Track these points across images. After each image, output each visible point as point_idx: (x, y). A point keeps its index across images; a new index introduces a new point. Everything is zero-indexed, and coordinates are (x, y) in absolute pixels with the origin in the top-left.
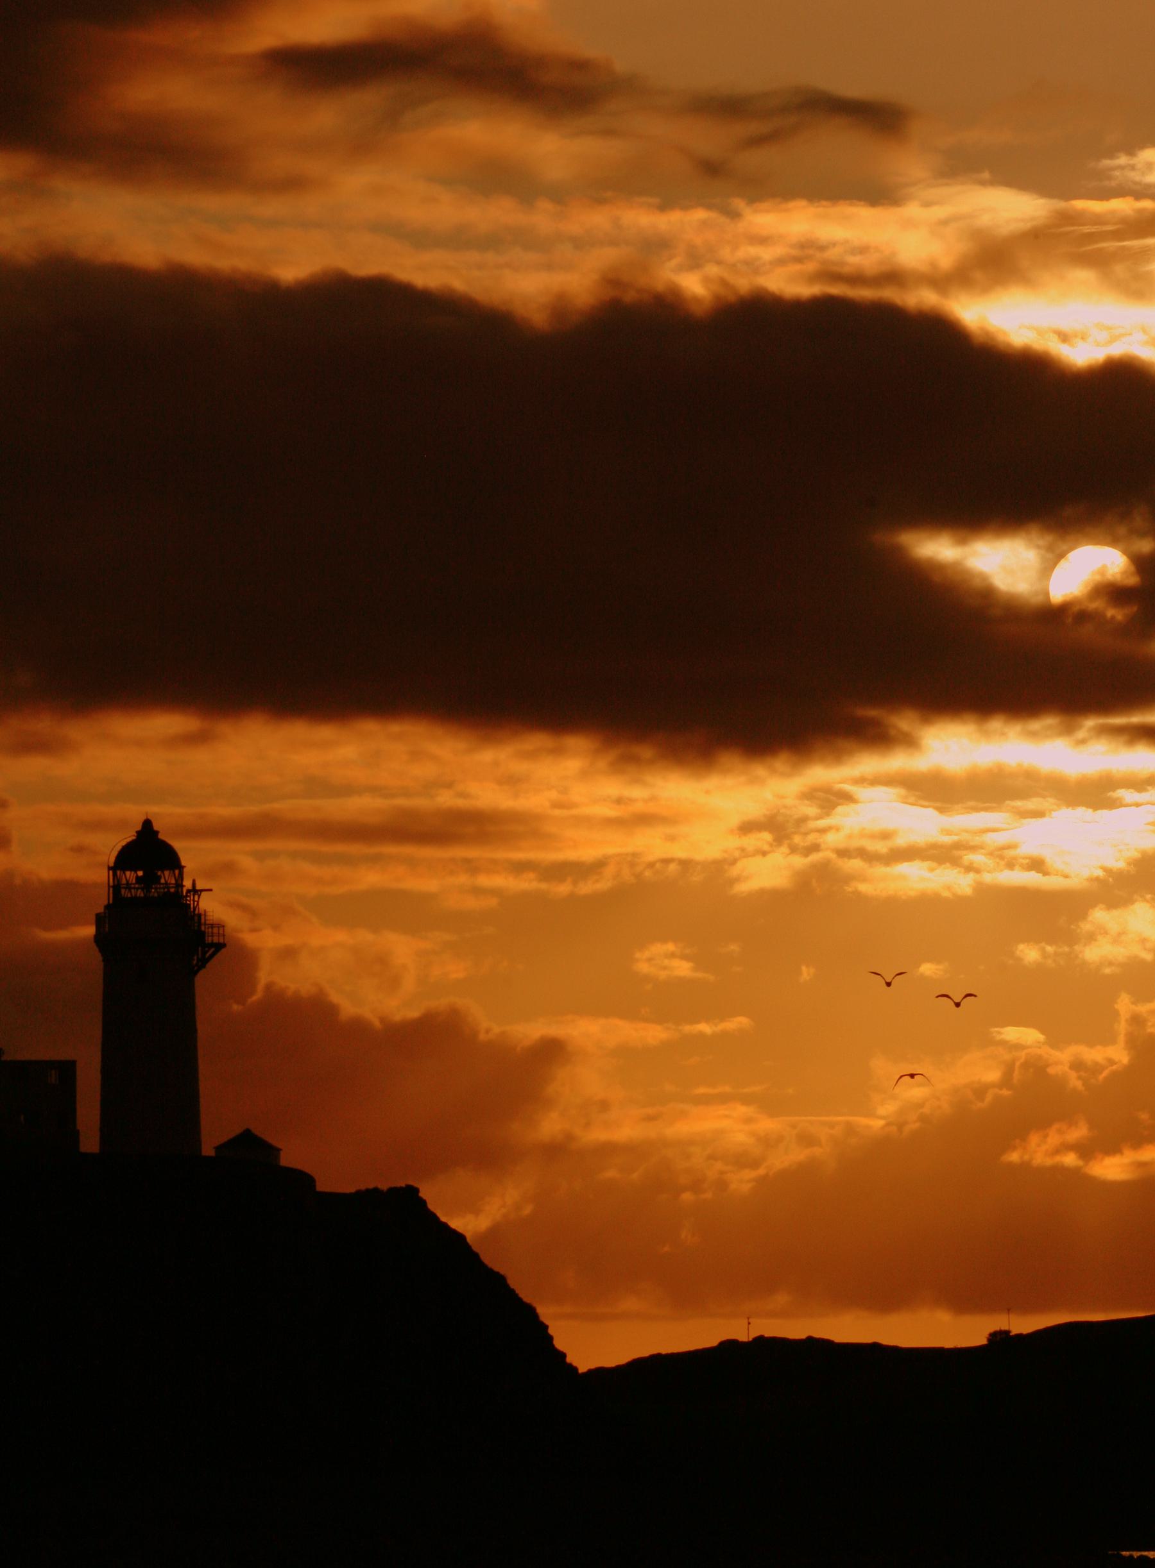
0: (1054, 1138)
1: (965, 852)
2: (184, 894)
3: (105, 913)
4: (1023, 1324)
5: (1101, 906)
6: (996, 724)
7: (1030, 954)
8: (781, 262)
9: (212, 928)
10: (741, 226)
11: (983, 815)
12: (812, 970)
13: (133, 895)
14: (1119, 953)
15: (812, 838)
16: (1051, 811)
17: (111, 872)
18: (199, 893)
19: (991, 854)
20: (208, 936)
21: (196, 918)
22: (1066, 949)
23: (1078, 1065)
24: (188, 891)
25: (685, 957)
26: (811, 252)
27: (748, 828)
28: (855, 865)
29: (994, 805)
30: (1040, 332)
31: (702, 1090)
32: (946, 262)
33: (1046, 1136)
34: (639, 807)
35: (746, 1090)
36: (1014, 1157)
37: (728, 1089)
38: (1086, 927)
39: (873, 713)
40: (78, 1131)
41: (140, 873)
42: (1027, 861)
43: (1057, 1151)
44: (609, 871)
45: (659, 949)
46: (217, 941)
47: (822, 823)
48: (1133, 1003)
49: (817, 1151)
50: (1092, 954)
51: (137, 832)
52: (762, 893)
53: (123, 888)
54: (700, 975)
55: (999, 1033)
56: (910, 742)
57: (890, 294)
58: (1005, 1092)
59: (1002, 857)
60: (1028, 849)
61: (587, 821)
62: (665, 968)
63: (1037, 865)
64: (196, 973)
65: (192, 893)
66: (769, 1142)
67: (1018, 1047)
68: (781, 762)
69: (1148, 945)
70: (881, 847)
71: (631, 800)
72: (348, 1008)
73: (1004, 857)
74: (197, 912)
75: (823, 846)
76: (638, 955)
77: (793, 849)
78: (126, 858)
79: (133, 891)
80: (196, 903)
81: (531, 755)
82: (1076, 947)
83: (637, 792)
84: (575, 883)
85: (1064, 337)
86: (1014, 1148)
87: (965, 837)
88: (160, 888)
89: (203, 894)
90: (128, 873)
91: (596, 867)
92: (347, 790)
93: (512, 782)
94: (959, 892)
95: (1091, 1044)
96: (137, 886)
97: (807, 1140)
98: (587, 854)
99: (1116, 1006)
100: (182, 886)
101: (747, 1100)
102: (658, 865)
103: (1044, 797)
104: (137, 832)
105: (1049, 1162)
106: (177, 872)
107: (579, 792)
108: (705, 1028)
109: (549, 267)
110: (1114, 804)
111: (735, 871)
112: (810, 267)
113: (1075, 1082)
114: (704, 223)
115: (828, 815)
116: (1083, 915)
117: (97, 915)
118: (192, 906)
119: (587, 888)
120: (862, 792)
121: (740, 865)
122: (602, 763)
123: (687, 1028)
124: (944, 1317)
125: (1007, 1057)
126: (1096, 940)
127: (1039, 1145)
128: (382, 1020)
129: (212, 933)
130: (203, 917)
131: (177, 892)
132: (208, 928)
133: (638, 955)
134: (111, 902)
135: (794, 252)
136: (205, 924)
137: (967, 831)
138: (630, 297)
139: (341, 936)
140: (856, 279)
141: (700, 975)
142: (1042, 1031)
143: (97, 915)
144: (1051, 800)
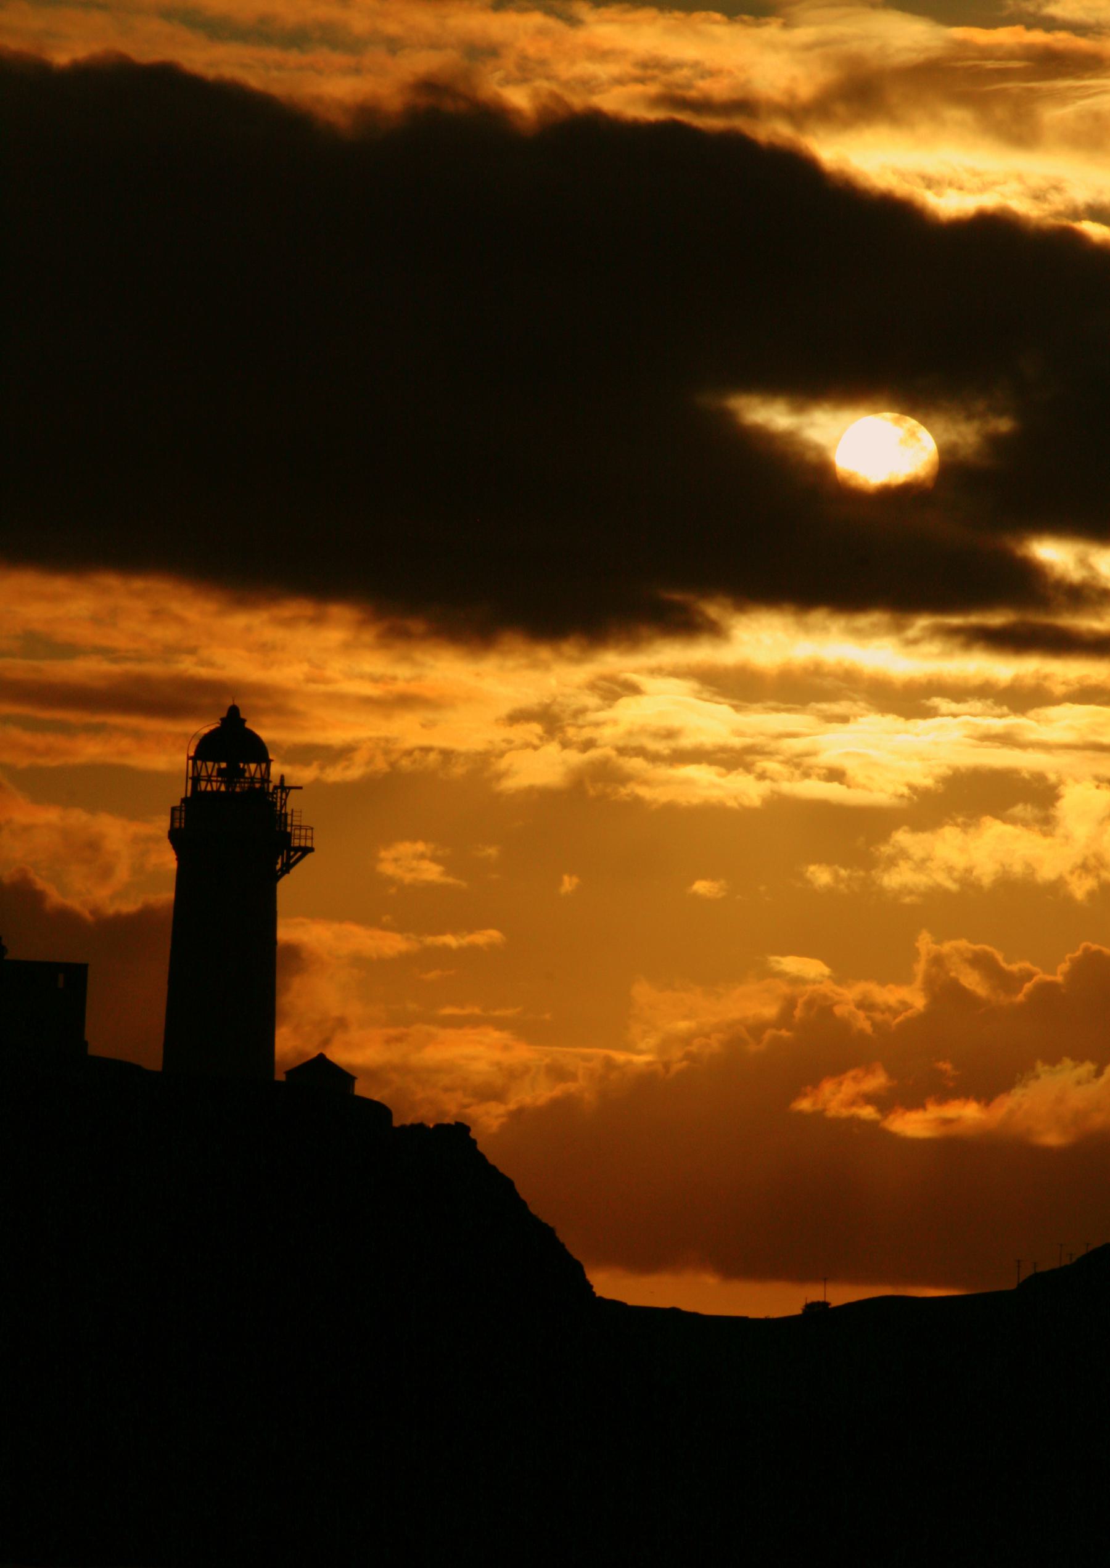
0: (848, 1088)
1: (758, 758)
2: (271, 790)
3: (181, 806)
4: (840, 1295)
5: (906, 828)
6: (818, 617)
7: (821, 876)
8: (619, 81)
9: (300, 829)
10: (580, 36)
11: (784, 716)
12: (575, 880)
13: (215, 789)
14: (920, 880)
15: (587, 733)
16: (855, 716)
17: (190, 762)
18: (288, 791)
19: (786, 762)
20: (294, 839)
21: (283, 817)
22: (862, 873)
23: (865, 1005)
24: (275, 788)
25: (435, 859)
26: (656, 72)
27: (517, 717)
28: (636, 764)
29: (798, 706)
30: (902, 175)
31: (449, 1011)
32: (806, 91)
33: (840, 1084)
34: (400, 687)
35: (497, 1013)
36: (805, 1105)
37: (477, 1011)
38: (886, 850)
39: (677, 597)
40: (86, 1043)
41: (223, 765)
42: (824, 771)
43: (852, 1103)
44: (360, 757)
45: (406, 848)
46: (298, 845)
47: (602, 715)
48: (933, 942)
49: (572, 1087)
50: (896, 878)
51: (222, 720)
52: (531, 790)
53: (203, 780)
54: (450, 880)
55: (778, 962)
56: (715, 631)
57: (738, 123)
58: (784, 1033)
59: (797, 766)
60: (829, 757)
61: (339, 700)
62: (412, 870)
63: (835, 775)
64: (278, 878)
65: (279, 790)
66: (514, 1074)
67: (797, 981)
68: (569, 648)
69: (956, 874)
70: (662, 747)
71: (394, 679)
72: (55, 897)
73: (800, 765)
74: (283, 812)
75: (599, 742)
76: (383, 854)
77: (565, 745)
78: (207, 749)
79: (214, 784)
80: (283, 801)
81: (289, 623)
82: (873, 872)
83: (403, 671)
84: (322, 768)
85: (930, 183)
86: (805, 1095)
87: (759, 740)
88: (244, 783)
89: (292, 792)
90: (210, 764)
91: (344, 753)
92: (71, 650)
93: (265, 649)
94: (746, 802)
95: (883, 983)
96: (220, 779)
97: (557, 1073)
98: (336, 737)
99: (917, 945)
100: (269, 781)
101: (500, 1024)
102: (417, 754)
103: (854, 701)
104: (222, 720)
105: (845, 1113)
106: (264, 766)
107: (336, 667)
108: (450, 940)
109: (357, 71)
110: (930, 713)
111: (503, 764)
112: (653, 89)
113: (862, 1023)
114: (541, 32)
115: (610, 706)
116: (884, 836)
117: (173, 809)
118: (279, 804)
119: (335, 774)
120: (646, 682)
121: (508, 756)
122: (368, 636)
123: (430, 940)
124: (710, 1281)
125: (785, 989)
126: (896, 865)
127: (834, 1094)
128: (92, 912)
129: (300, 835)
130: (289, 818)
131: (262, 788)
132: (295, 829)
133: (383, 854)
134: (189, 795)
135: (637, 72)
136: (292, 825)
137: (762, 734)
138: (449, 105)
139: (51, 815)
140: (704, 106)
141: (450, 880)
142: (828, 964)
143: (173, 809)
144: (862, 704)
